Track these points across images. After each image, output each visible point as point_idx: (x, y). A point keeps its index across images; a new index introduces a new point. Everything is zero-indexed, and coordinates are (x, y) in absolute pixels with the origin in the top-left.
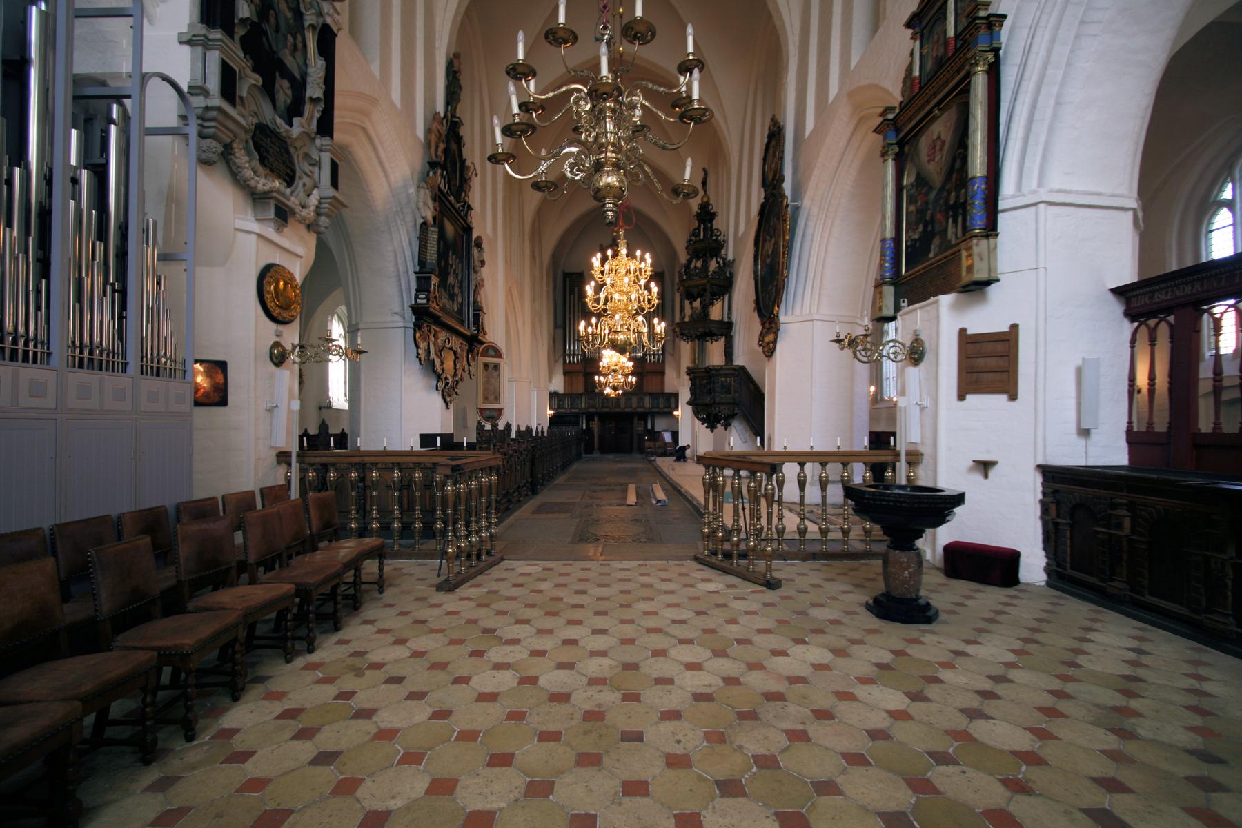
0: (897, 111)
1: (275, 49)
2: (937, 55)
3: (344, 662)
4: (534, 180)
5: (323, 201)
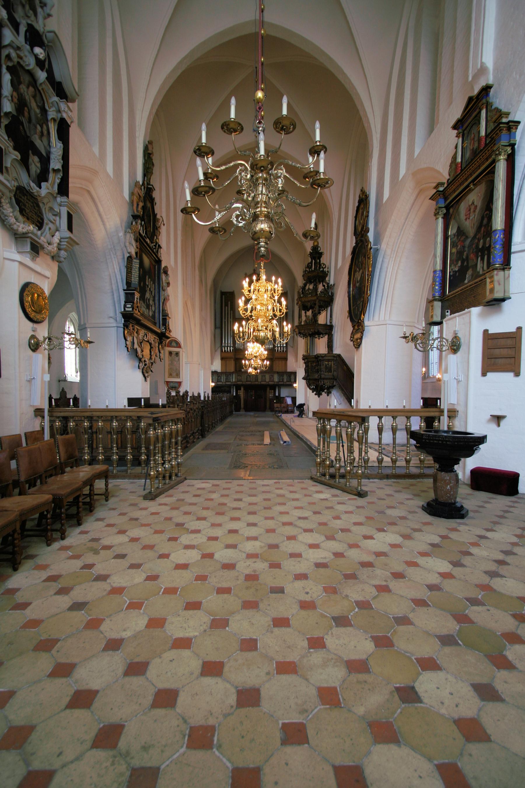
0: (446, 185)
1: (28, 135)
2: (473, 148)
3: (85, 545)
4: (211, 226)
5: (62, 240)
